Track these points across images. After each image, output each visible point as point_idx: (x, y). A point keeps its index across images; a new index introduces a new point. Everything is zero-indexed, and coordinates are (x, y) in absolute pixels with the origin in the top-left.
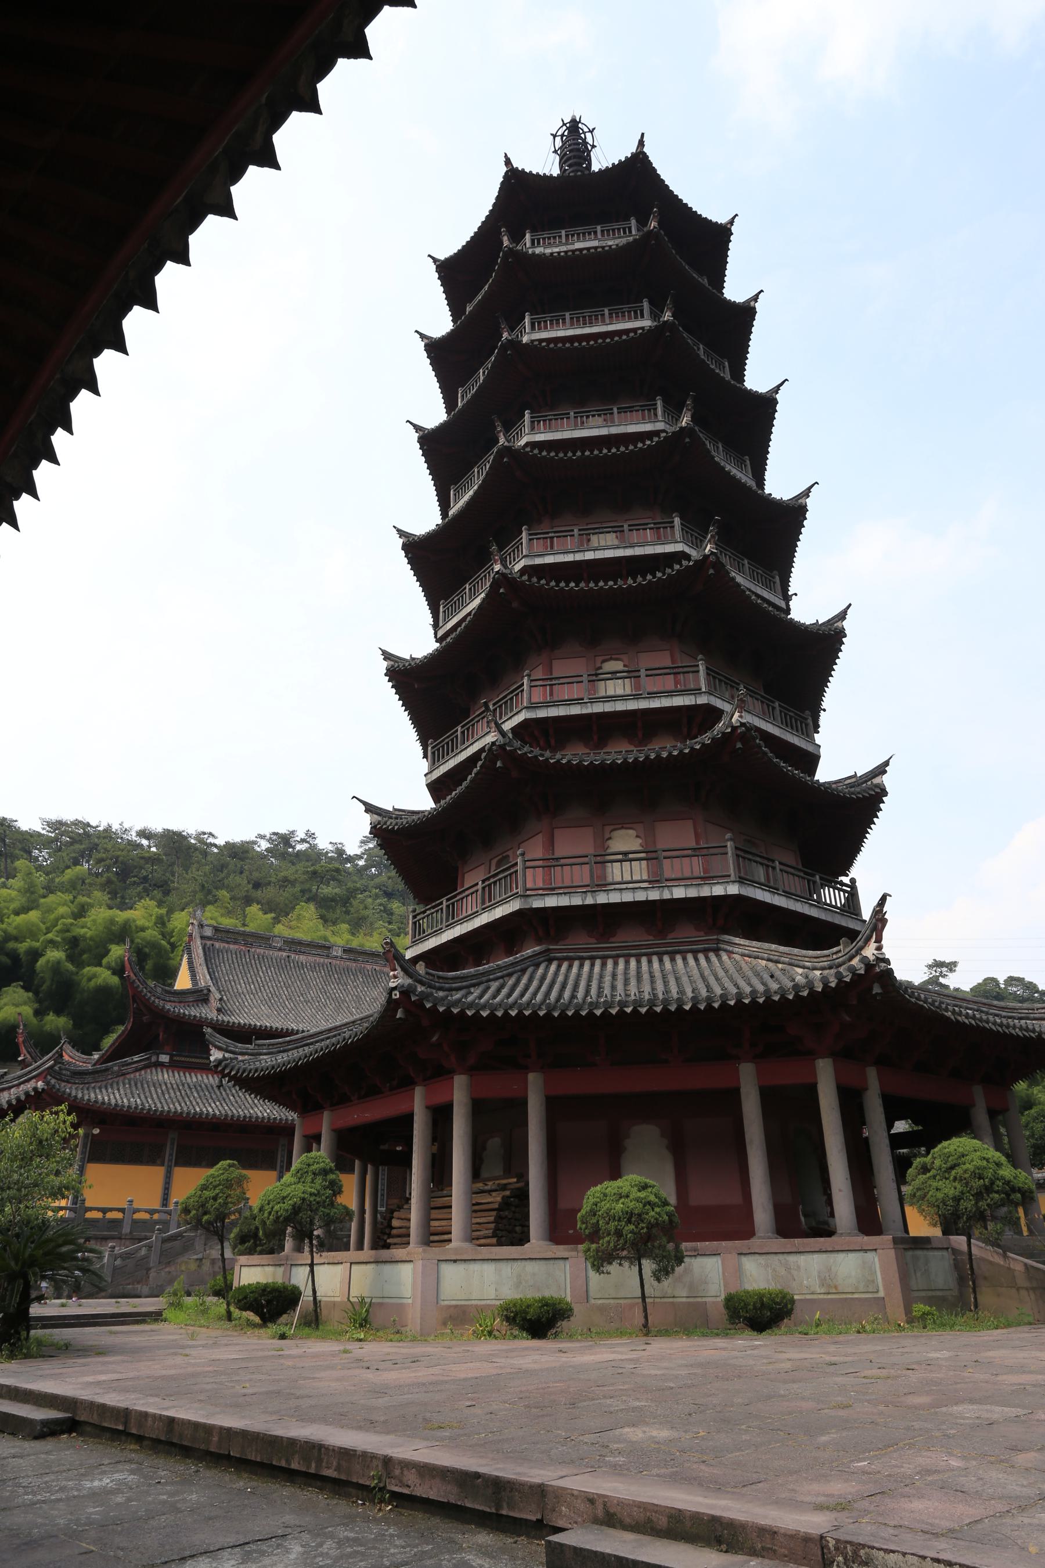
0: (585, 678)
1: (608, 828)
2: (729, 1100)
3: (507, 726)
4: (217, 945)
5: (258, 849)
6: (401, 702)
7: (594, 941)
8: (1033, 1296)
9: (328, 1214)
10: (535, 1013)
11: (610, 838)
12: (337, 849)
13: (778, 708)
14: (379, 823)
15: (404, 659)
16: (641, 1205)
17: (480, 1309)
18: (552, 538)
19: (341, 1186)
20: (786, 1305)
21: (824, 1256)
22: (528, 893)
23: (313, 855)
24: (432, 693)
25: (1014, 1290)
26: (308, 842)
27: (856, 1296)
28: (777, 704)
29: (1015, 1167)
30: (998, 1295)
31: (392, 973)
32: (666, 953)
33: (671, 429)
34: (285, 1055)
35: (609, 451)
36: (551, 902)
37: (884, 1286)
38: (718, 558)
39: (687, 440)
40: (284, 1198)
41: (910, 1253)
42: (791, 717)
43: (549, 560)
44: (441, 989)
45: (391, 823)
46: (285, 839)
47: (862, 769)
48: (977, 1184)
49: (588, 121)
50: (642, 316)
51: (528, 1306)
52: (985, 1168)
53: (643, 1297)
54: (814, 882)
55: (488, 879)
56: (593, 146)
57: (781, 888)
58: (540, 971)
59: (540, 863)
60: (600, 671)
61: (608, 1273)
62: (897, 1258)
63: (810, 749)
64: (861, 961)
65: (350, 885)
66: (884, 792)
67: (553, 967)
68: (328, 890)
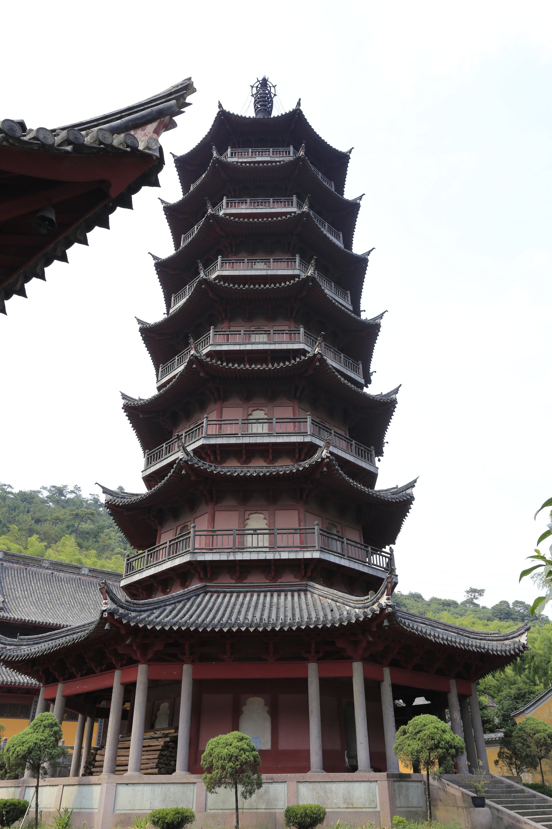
0: (240, 422)
1: (247, 513)
2: (302, 685)
3: (190, 449)
4: (5, 564)
5: (41, 496)
7: (233, 581)
8: (465, 812)
9: (51, 753)
10: (188, 629)
11: (248, 519)
12: (94, 498)
13: (354, 444)
14: (110, 501)
15: (135, 400)
16: (238, 750)
17: (138, 816)
19: (61, 735)
20: (320, 815)
21: (347, 784)
22: (196, 551)
23: (78, 502)
24: (152, 421)
25: (455, 808)
26: (75, 493)
27: (363, 810)
28: (353, 442)
29: (455, 734)
30: (447, 812)
31: (104, 601)
32: (276, 591)
33: (303, 276)
34: (36, 646)
35: (265, 286)
36: (209, 557)
37: (380, 804)
38: (322, 356)
39: (311, 284)
40: (23, 743)
41: (397, 784)
42: (362, 450)
43: (225, 348)
44: (134, 611)
45: (118, 501)
46: (60, 491)
47: (401, 484)
48: (430, 743)
49: (272, 81)
50: (292, 205)
51: (167, 814)
52: (436, 733)
53: (237, 809)
54: (367, 551)
55: (175, 539)
57: (345, 553)
58: (199, 599)
59: (205, 533)
60: (251, 417)
61: (216, 793)
62: (388, 787)
63: (372, 469)
64: (378, 606)
65: (101, 523)
66: (412, 498)
67: (207, 597)
68: (86, 526)
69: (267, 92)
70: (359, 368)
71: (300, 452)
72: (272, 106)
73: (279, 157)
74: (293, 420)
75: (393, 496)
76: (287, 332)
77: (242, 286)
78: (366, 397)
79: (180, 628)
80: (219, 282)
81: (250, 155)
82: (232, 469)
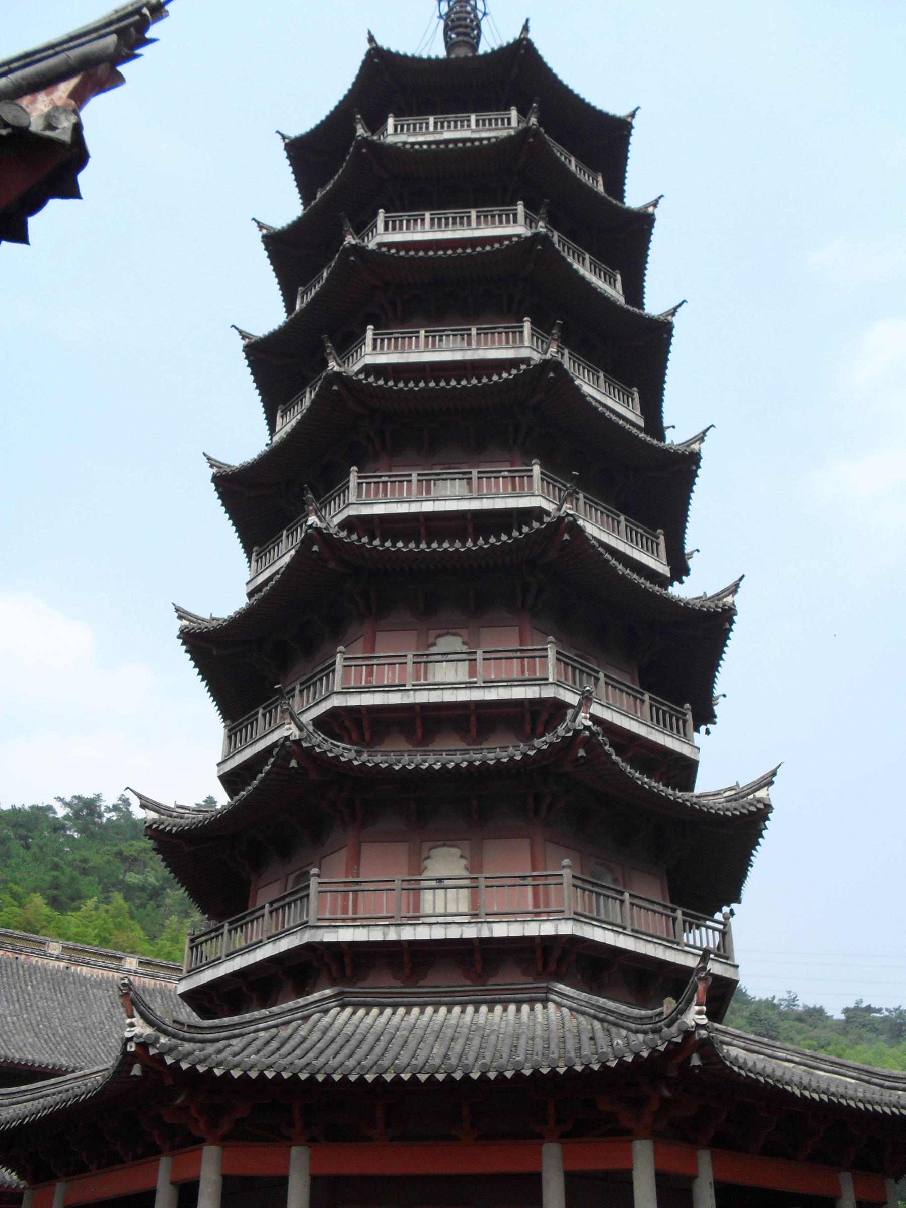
0: (397, 885)
3: (306, 718)
6: (197, 670)
7: (399, 983)
11: (428, 857)
15: (204, 620)
18: (385, 483)
24: (239, 662)
31: (128, 1021)
33: (536, 357)
35: (459, 383)
45: (170, 825)
47: (746, 780)
50: (515, 221)
55: (283, 898)
56: (485, 14)
57: (628, 924)
60: (433, 650)
63: (685, 750)
66: (768, 808)
69: (469, 8)
70: (658, 544)
71: (534, 719)
72: (479, 36)
73: (489, 130)
74: (519, 654)
75: (728, 805)
76: (506, 473)
77: (411, 384)
78: (674, 605)
79: (278, 1075)
80: (366, 378)
81: (431, 129)
82: (392, 758)
